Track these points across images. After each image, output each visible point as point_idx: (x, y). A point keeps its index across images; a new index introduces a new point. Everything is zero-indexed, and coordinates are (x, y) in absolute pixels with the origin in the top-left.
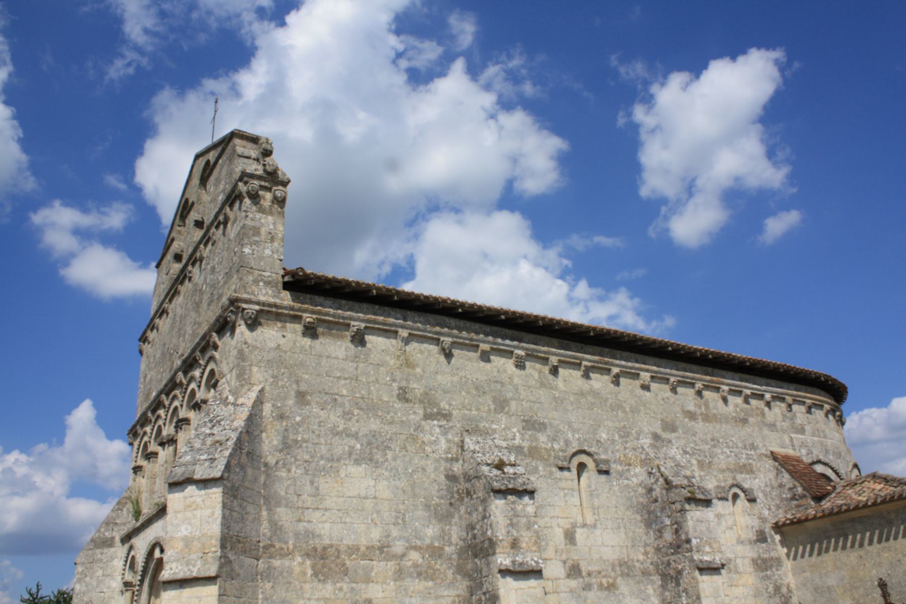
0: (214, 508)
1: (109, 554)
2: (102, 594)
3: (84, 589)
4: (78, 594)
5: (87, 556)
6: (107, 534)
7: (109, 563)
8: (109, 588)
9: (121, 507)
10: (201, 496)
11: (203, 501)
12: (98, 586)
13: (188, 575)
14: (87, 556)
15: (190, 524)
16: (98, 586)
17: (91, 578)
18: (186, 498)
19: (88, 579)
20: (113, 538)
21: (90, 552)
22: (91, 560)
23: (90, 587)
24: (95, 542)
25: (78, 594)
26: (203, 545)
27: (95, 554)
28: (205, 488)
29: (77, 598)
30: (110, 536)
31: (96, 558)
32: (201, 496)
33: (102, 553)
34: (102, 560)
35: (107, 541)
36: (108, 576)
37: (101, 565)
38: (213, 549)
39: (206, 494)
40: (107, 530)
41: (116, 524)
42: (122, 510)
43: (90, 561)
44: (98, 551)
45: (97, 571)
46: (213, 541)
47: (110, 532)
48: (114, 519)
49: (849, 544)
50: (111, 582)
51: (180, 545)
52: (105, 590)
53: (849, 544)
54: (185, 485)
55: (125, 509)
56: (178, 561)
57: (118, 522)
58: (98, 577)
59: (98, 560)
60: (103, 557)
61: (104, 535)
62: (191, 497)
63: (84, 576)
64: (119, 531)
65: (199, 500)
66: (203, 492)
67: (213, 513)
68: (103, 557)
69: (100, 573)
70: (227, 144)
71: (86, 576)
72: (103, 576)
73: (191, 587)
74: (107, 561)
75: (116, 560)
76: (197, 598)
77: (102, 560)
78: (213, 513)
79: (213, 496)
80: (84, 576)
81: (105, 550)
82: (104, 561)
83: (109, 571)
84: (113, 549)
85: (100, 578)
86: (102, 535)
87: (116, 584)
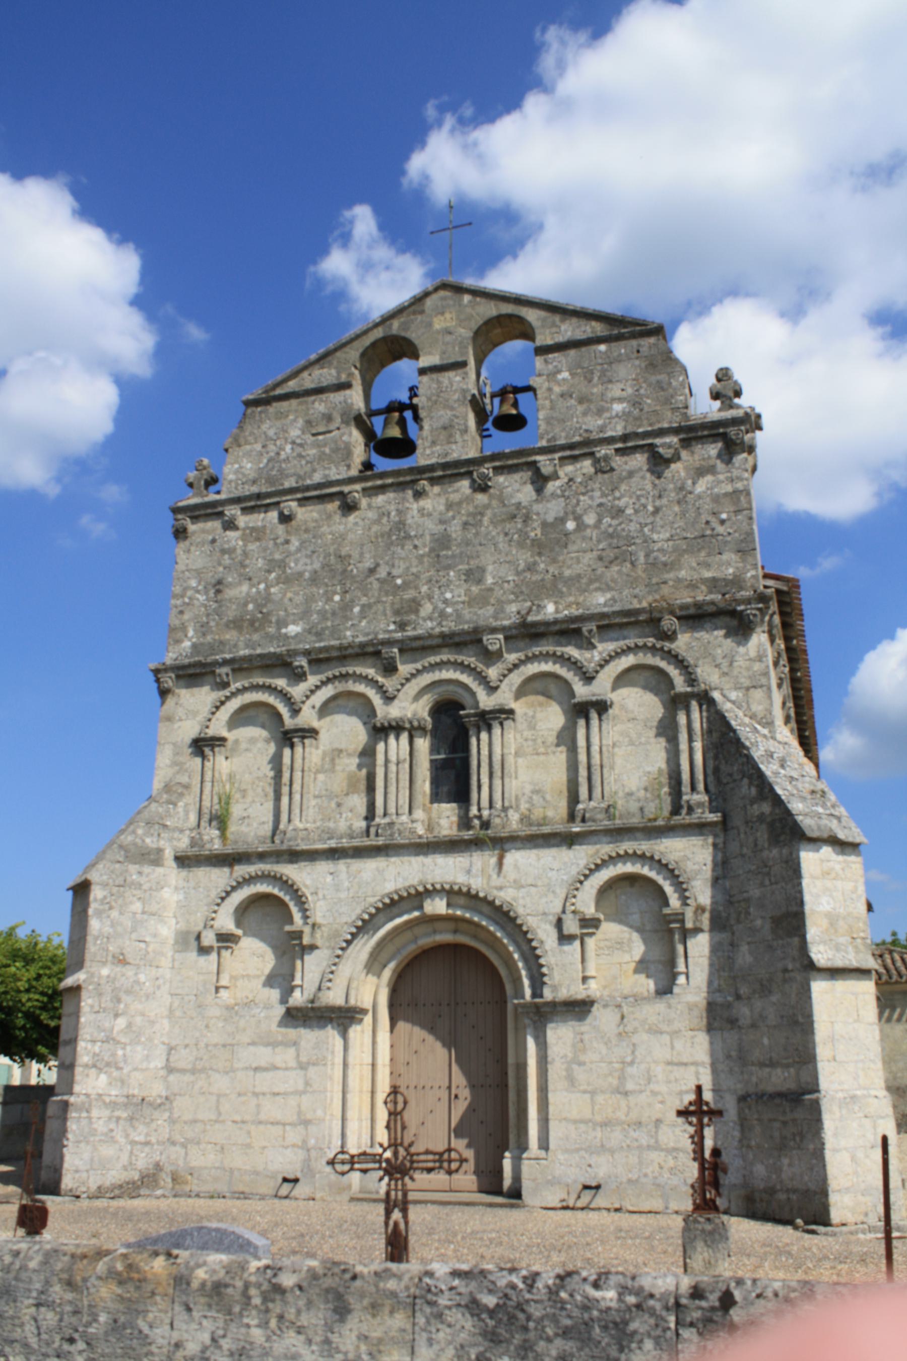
0: (856, 881)
1: (152, 877)
2: (143, 945)
3: (107, 930)
4: (96, 938)
5: (112, 872)
6: (148, 840)
7: (154, 893)
8: (155, 936)
9: (173, 798)
10: (839, 862)
11: (843, 869)
12: (134, 929)
13: (839, 963)
14: (112, 872)
15: (831, 896)
16: (134, 929)
17: (121, 913)
18: (822, 861)
19: (114, 914)
20: (160, 851)
21: (117, 866)
22: (120, 881)
23: (119, 929)
24: (126, 851)
25: (96, 938)
26: (851, 927)
27: (127, 871)
28: (843, 853)
29: (95, 944)
30: (154, 846)
31: (129, 879)
32: (839, 862)
33: (140, 873)
34: (141, 885)
35: (149, 854)
36: (154, 915)
37: (138, 893)
38: (862, 935)
39: (845, 861)
40: (148, 834)
41: (165, 826)
42: (175, 804)
43: (117, 883)
44: (133, 868)
45: (131, 903)
46: (861, 925)
47: (155, 839)
48: (162, 818)
49: (896, 1016)
50: (159, 927)
51: (825, 923)
52: (147, 939)
53: (896, 1016)
54: (819, 844)
55: (181, 804)
56: (825, 943)
57: (168, 823)
58: (135, 913)
59: (133, 883)
60: (143, 880)
61: (143, 841)
62: (829, 861)
63: (107, 907)
64: (171, 839)
65: (838, 867)
66: (841, 858)
67: (856, 888)
68: (143, 880)
69: (137, 906)
70: (634, 336)
71: (111, 908)
72: (144, 913)
73: (844, 979)
74: (151, 889)
75: (166, 889)
76: (853, 994)
77: (141, 885)
78: (856, 888)
79: (853, 866)
80: (107, 907)
81: (147, 869)
82: (145, 887)
83: (154, 907)
84: (160, 870)
85: (138, 916)
86: (138, 841)
87: (167, 930)
